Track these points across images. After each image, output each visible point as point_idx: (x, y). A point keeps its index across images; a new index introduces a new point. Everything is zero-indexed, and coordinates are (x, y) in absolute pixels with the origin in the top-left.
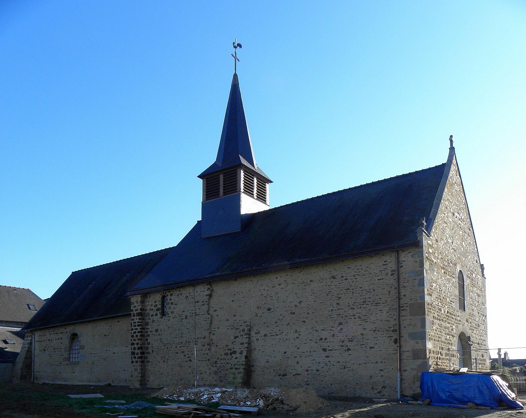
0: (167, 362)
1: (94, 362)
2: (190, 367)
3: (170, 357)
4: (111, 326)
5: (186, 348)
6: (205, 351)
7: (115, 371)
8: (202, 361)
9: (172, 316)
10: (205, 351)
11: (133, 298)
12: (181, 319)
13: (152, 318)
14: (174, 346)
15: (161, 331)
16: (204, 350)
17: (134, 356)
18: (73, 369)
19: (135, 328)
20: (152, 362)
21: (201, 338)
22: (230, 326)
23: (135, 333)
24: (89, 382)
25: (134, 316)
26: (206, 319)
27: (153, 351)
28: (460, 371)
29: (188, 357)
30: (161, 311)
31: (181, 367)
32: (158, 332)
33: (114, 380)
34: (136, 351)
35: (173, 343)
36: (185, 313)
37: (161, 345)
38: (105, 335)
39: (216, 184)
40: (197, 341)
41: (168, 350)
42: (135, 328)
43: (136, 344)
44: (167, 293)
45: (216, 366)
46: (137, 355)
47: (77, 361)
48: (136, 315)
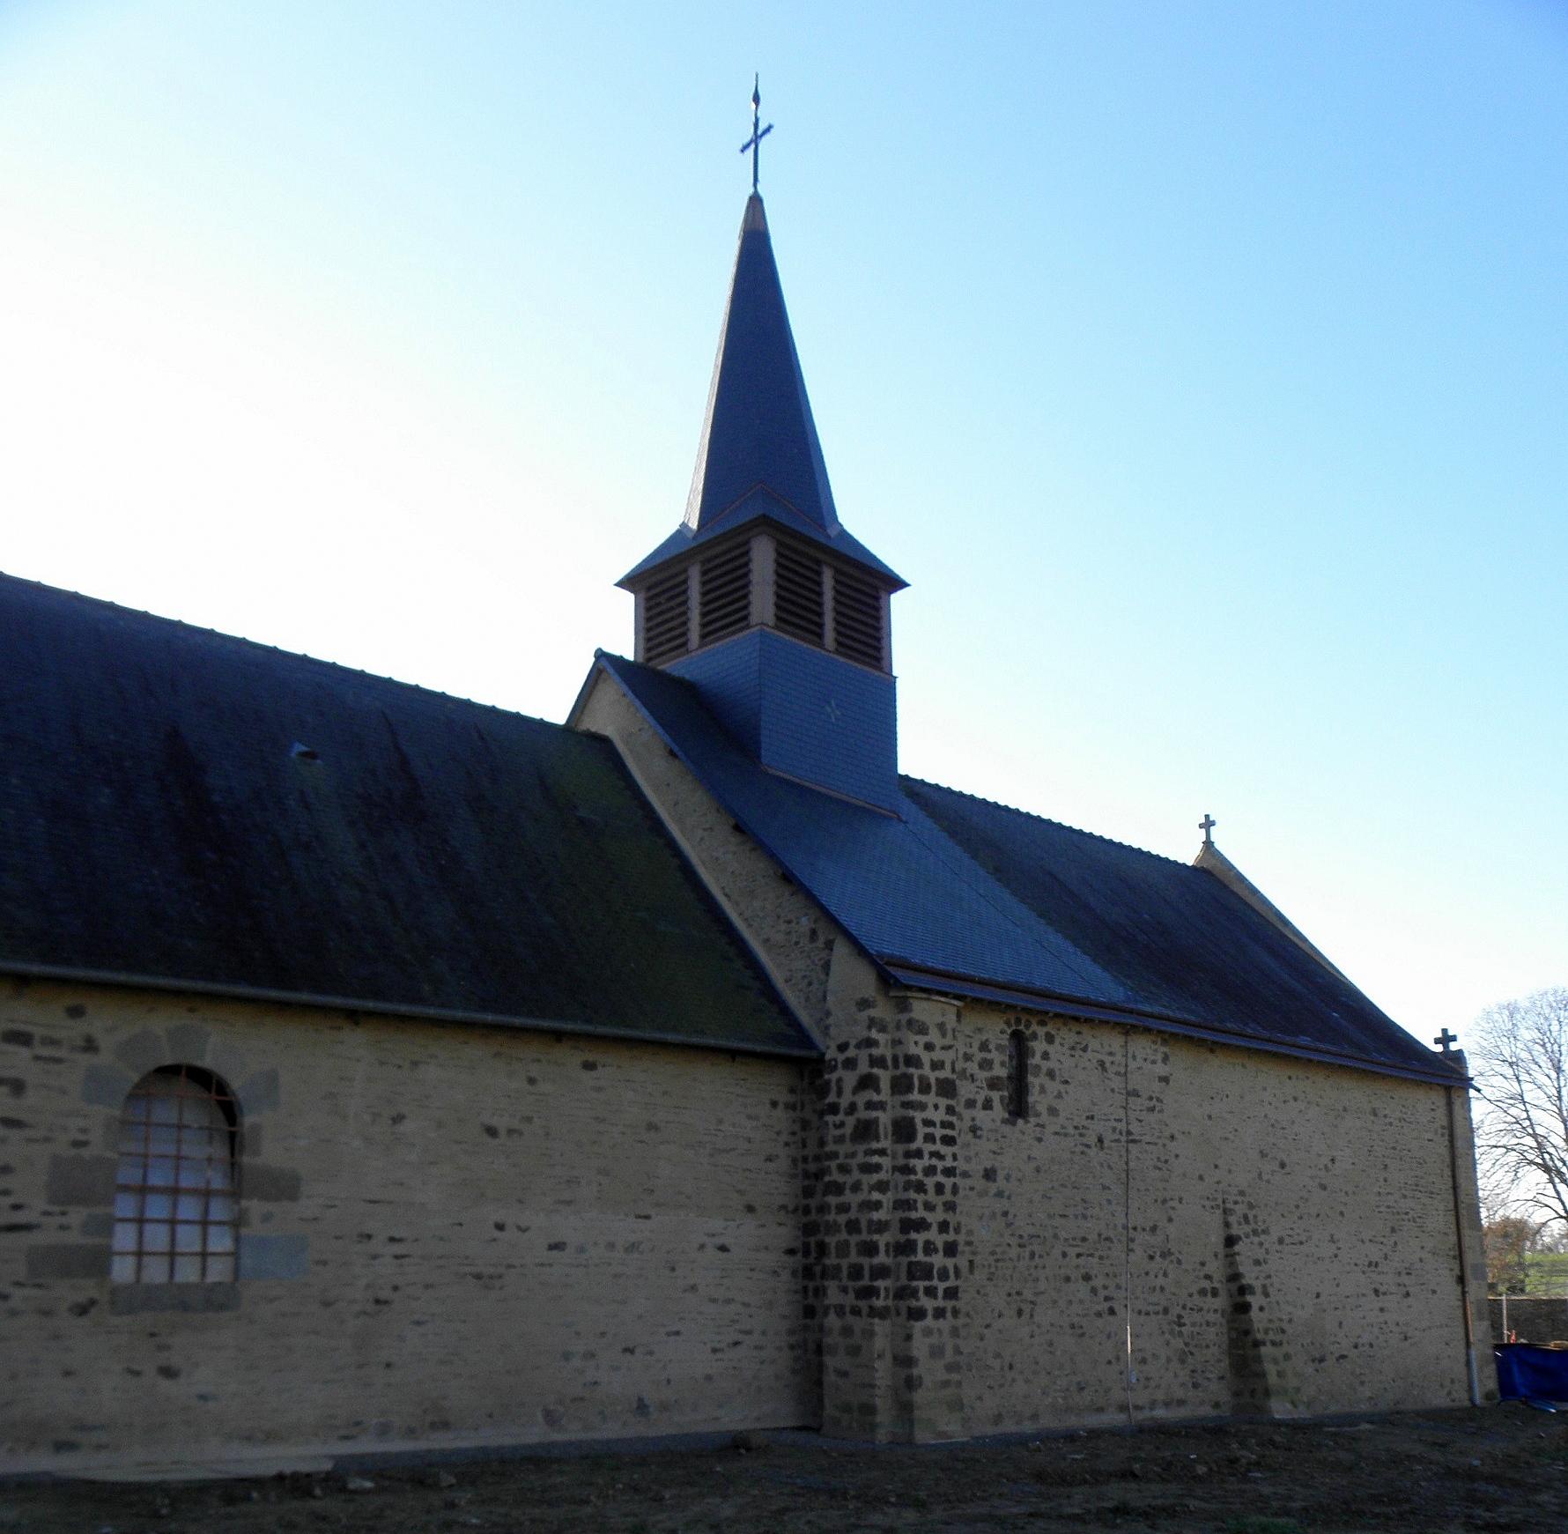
0: (1032, 1316)
1: (385, 1294)
2: (1109, 1336)
3: (1042, 1293)
4: (532, 1081)
5: (1096, 1260)
6: (1156, 1276)
7: (567, 1356)
8: (1147, 1314)
9: (1053, 1125)
10: (1156, 1276)
11: (930, 1003)
12: (1083, 1144)
13: (967, 1114)
14: (1057, 1252)
15: (1008, 1178)
16: (1152, 1275)
17: (927, 1283)
19: (932, 1148)
20: (968, 1315)
21: (1144, 1230)
22: (1208, 1198)
23: (930, 1171)
24: (346, 1438)
25: (925, 1089)
26: (1159, 1165)
27: (971, 1262)
29: (1107, 1299)
30: (1006, 1094)
31: (1083, 1335)
32: (995, 1181)
33: (561, 1409)
34: (938, 1260)
35: (1056, 1236)
36: (1096, 1127)
37: (1008, 1239)
38: (492, 1132)
40: (1133, 1240)
41: (1033, 1264)
42: (932, 1148)
43: (935, 1228)
44: (1035, 1027)
45: (1180, 1334)
46: (940, 1279)
48: (934, 1089)
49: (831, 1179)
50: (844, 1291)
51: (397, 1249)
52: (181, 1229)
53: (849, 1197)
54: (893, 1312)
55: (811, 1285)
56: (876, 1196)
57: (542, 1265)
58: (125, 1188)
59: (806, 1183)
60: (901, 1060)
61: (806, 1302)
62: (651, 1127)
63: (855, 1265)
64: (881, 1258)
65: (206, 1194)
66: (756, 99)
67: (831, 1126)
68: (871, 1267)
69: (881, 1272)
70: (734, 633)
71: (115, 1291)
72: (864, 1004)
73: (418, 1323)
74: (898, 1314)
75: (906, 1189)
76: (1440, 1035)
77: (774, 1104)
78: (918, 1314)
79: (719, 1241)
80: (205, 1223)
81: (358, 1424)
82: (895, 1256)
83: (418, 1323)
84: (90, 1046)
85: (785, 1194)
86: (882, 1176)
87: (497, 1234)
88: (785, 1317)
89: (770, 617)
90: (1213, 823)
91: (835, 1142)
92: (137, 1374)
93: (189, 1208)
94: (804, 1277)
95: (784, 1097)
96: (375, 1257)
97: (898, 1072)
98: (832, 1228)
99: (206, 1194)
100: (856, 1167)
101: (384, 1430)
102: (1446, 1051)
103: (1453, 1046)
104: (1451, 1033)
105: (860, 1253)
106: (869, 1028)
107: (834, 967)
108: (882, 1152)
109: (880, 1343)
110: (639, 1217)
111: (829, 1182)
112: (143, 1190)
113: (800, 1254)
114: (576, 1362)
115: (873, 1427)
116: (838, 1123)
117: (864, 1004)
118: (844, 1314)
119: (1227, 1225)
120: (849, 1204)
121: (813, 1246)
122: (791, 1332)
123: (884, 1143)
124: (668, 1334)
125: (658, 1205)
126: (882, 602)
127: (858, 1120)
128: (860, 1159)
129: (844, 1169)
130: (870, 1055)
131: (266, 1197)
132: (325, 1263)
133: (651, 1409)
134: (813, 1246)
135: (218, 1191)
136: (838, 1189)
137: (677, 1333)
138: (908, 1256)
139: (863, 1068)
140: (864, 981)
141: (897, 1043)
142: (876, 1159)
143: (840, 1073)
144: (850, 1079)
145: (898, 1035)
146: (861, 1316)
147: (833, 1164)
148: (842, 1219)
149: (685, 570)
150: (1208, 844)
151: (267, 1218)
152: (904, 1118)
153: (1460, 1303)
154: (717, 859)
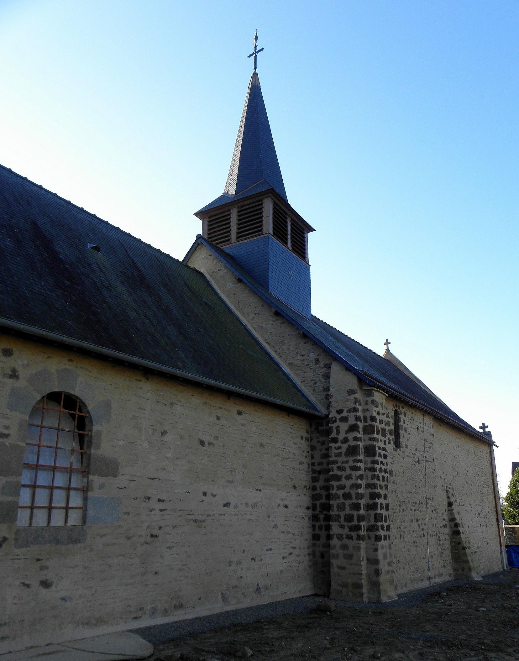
1: (156, 531)
4: (218, 418)
7: (230, 564)
18: (42, 568)
28: (494, 446)
38: (202, 443)
39: (214, 232)
44: (401, 409)
47: (61, 523)
49: (333, 473)
50: (342, 528)
51: (161, 506)
52: (38, 491)
53: (344, 482)
55: (317, 524)
56: (359, 481)
57: (221, 515)
58: (28, 466)
59: (314, 475)
60: (369, 418)
61: (314, 533)
62: (262, 445)
64: (362, 512)
65: (70, 471)
66: (256, 38)
67: (333, 448)
68: (358, 516)
69: (361, 518)
70: (254, 236)
71: (18, 531)
72: (351, 392)
73: (170, 548)
74: (369, 538)
76: (481, 425)
77: (302, 438)
78: (378, 538)
79: (285, 502)
80: (68, 489)
81: (141, 609)
83: (170, 548)
84: (14, 375)
86: (361, 472)
87: (203, 498)
88: (306, 540)
89: (271, 230)
90: (389, 343)
91: (336, 456)
92: (28, 586)
93: (60, 480)
94: (313, 520)
95: (305, 435)
96: (151, 510)
97: (367, 424)
98: (337, 497)
99: (70, 471)
100: (348, 468)
101: (154, 611)
102: (485, 432)
103: (487, 430)
104: (486, 425)
105: (351, 509)
106: (355, 403)
107: (333, 376)
108: (360, 461)
109: (363, 553)
110: (257, 490)
111: (332, 475)
112: (36, 468)
113: (311, 509)
114: (234, 567)
115: (361, 595)
116: (337, 447)
117: (351, 392)
118: (343, 538)
119: (448, 497)
120: (345, 485)
121: (318, 506)
122: (309, 547)
123: (361, 457)
124: (267, 550)
125: (264, 484)
126: (305, 235)
127: (349, 446)
128: (351, 464)
129: (340, 468)
130: (356, 416)
131: (101, 475)
132: (128, 514)
133: (262, 590)
134: (318, 506)
135: (76, 469)
136: (339, 478)
137: (271, 549)
138: (375, 510)
139: (352, 421)
140: (353, 383)
141: (365, 411)
143: (338, 423)
144: (344, 427)
145: (366, 407)
146: (353, 540)
147: (335, 466)
148: (341, 492)
149: (230, 210)
150: (388, 350)
151: (102, 486)
152: (371, 445)
153: (497, 529)
154: (262, 327)
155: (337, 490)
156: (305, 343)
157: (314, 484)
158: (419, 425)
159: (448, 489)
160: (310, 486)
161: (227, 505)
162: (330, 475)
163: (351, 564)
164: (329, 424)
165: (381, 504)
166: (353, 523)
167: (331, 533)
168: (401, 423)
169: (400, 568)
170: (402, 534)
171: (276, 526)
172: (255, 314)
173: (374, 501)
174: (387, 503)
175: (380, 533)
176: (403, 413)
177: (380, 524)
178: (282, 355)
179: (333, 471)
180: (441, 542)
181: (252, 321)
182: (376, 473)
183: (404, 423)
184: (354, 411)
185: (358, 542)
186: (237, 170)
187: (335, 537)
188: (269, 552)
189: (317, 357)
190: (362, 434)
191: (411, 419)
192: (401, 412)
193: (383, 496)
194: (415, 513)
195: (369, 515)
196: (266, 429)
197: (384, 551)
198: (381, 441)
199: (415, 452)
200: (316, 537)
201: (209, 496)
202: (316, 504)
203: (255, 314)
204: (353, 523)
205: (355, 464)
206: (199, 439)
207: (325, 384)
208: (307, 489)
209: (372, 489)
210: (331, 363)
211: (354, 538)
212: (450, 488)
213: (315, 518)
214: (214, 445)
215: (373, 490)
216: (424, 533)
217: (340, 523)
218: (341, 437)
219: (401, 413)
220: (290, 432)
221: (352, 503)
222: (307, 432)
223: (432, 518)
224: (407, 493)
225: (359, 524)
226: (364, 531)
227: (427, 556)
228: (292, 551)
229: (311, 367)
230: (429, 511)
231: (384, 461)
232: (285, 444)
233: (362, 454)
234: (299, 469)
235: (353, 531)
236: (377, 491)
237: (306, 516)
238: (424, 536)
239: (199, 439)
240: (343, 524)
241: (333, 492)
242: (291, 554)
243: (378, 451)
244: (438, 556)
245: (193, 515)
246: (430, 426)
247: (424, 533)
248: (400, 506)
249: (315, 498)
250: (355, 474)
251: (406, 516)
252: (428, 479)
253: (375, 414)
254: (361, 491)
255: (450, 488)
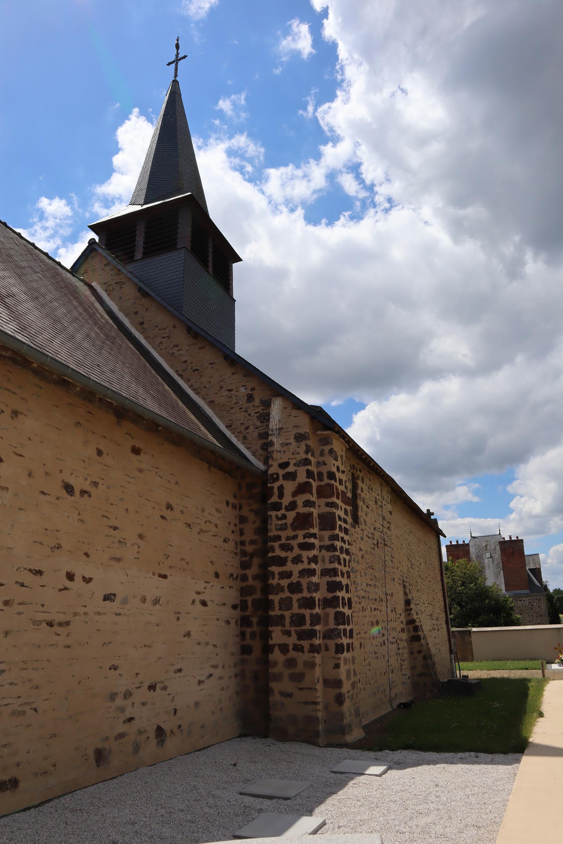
4: (100, 453)
7: (113, 697)
28: (441, 537)
38: (69, 489)
53: (289, 567)
54: (323, 648)
55: (248, 630)
56: (313, 566)
57: (99, 613)
60: (325, 475)
61: (244, 643)
63: (298, 615)
67: (274, 518)
69: (316, 620)
75: (331, 562)
77: (228, 503)
78: (340, 649)
79: (202, 597)
82: (324, 608)
85: (232, 566)
87: (68, 584)
91: (277, 530)
94: (242, 625)
97: (323, 483)
98: (280, 589)
108: (314, 536)
113: (239, 609)
114: (119, 701)
116: (280, 516)
121: (250, 603)
122: (235, 665)
123: (315, 530)
127: (298, 514)
128: (300, 540)
129: (286, 548)
136: (282, 562)
137: (180, 670)
139: (302, 477)
141: (318, 464)
142: (312, 540)
143: (281, 482)
144: (290, 487)
145: (321, 459)
146: (303, 652)
147: (276, 545)
154: (173, 354)
155: (279, 579)
156: (233, 374)
157: (243, 572)
158: (378, 497)
159: (405, 583)
160: (238, 575)
161: (108, 598)
162: (269, 557)
163: (301, 689)
164: (268, 484)
165: (343, 598)
166: (303, 628)
167: (271, 642)
168: (359, 491)
169: (361, 690)
170: (363, 641)
171: (188, 634)
172: (164, 338)
173: (335, 594)
174: (350, 597)
175: (342, 642)
176: (361, 479)
177: (342, 627)
178: (199, 391)
179: (273, 552)
180: (400, 651)
181: (159, 347)
182: (337, 553)
183: (362, 491)
184: (305, 465)
185: (311, 655)
186: (143, 201)
187: (276, 649)
188: (179, 674)
189: (250, 392)
190: (316, 498)
191: (369, 488)
192: (359, 475)
193: (344, 586)
194: (374, 613)
195: (327, 615)
196: (176, 483)
197: (347, 667)
198: (341, 509)
199: (373, 531)
200: (246, 650)
201: (78, 584)
202: (246, 601)
203: (164, 338)
204: (303, 628)
205: (307, 540)
206: (63, 481)
207: (262, 428)
208: (233, 580)
209: (330, 577)
210: (271, 400)
211: (306, 649)
212: (407, 583)
213: (245, 622)
214: (90, 496)
215: (333, 579)
216: (384, 640)
217: (284, 628)
218: (286, 501)
219: (359, 478)
220: (212, 493)
221: (303, 597)
222: (235, 497)
223: (391, 620)
224: (367, 585)
225: (313, 628)
226: (320, 638)
227: (388, 671)
228: (212, 671)
229: (242, 405)
230: (389, 611)
231: (346, 538)
232: (203, 510)
233: (316, 527)
234: (222, 549)
235: (304, 640)
236: (339, 579)
237: (232, 618)
238: (384, 644)
239: (63, 481)
240: (289, 629)
241: (274, 582)
242: (211, 675)
243: (339, 523)
244: (398, 670)
245: (46, 612)
246: (388, 500)
247: (384, 640)
248: (360, 603)
249: (244, 592)
250: (306, 554)
251: (366, 617)
252: (387, 569)
253: (334, 470)
254: (315, 579)
255: (407, 583)
